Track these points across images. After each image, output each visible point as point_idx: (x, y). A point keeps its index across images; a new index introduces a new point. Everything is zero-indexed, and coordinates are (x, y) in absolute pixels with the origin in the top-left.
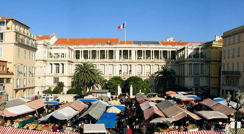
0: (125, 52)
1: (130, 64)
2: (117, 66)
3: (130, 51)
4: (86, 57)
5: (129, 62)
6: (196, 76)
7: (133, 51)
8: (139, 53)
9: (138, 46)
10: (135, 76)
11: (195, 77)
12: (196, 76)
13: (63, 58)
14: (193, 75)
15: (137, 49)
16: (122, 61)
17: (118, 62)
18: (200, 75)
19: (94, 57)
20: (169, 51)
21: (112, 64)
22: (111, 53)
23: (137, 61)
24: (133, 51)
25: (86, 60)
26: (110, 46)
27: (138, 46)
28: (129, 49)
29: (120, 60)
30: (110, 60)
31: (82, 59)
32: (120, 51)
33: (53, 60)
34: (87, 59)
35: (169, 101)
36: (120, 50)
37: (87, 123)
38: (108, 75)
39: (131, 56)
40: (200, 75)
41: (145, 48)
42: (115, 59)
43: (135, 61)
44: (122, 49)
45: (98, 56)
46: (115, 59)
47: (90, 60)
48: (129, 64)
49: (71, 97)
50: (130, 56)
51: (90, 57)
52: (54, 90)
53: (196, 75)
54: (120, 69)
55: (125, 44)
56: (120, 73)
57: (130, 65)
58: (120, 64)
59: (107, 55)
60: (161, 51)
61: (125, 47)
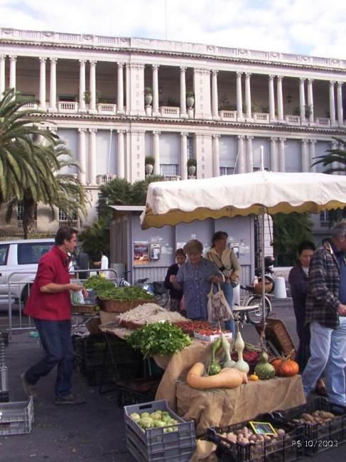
1: (193, 129)
2: (134, 137)
3: (190, 72)
5: (185, 122)
7: (202, 71)
8: (226, 83)
10: (99, 192)
16: (156, 114)
17: (139, 120)
21: (110, 126)
22: (108, 76)
23: (217, 117)
24: (202, 71)
25: (73, 107)
29: (149, 109)
30: (102, 111)
32: (148, 69)
36: (146, 65)
37: (278, 411)
38: (94, 183)
39: (194, 96)
41: (92, 49)
42: (125, 104)
44: (156, 62)
46: (125, 104)
48: (185, 130)
50: (187, 96)
51: (88, 92)
52: (93, 233)
54: (148, 155)
57: (191, 137)
58: (149, 127)
59: (88, 84)
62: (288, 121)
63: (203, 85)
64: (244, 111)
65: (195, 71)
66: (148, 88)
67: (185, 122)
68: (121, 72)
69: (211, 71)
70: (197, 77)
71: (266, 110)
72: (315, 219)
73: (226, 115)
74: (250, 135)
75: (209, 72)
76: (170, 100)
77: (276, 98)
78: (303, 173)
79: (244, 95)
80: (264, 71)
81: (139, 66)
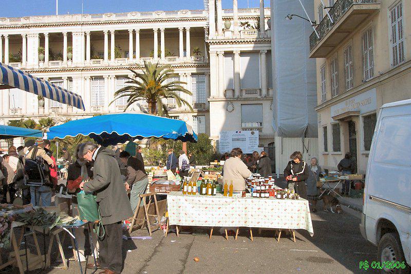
0: (56, 39)
3: (70, 35)
4: (147, 51)
5: (64, 70)
6: (250, 96)
8: (96, 38)
9: (11, 21)
11: (246, 99)
12: (250, 96)
13: (70, 62)
14: (237, 93)
15: (89, 29)
18: (264, 92)
19: (172, 51)
20: (109, 33)
26: (13, 23)
27: (11, 21)
28: (64, 30)
31: (135, 59)
32: (42, 37)
33: (114, 64)
34: (60, 62)
35: (75, 190)
40: (264, 92)
43: (81, 65)
44: (46, 31)
45: (185, 50)
47: (160, 59)
48: (65, 75)
49: (303, 221)
51: (159, 51)
53: (248, 92)
55: (54, 14)
56: (39, 105)
60: (109, 33)
61: (54, 22)
62: (90, 63)
63: (80, 46)
64: (109, 58)
65: (73, 34)
66: (41, 48)
67: (64, 70)
68: (24, 40)
69: (85, 33)
70: (74, 38)
71: (101, 55)
72: (20, 168)
73: (170, 60)
74: (188, 72)
75: (84, 34)
76: (55, 55)
77: (135, 45)
78: (210, 110)
79: (109, 46)
80: (175, 25)
81: (78, 33)
